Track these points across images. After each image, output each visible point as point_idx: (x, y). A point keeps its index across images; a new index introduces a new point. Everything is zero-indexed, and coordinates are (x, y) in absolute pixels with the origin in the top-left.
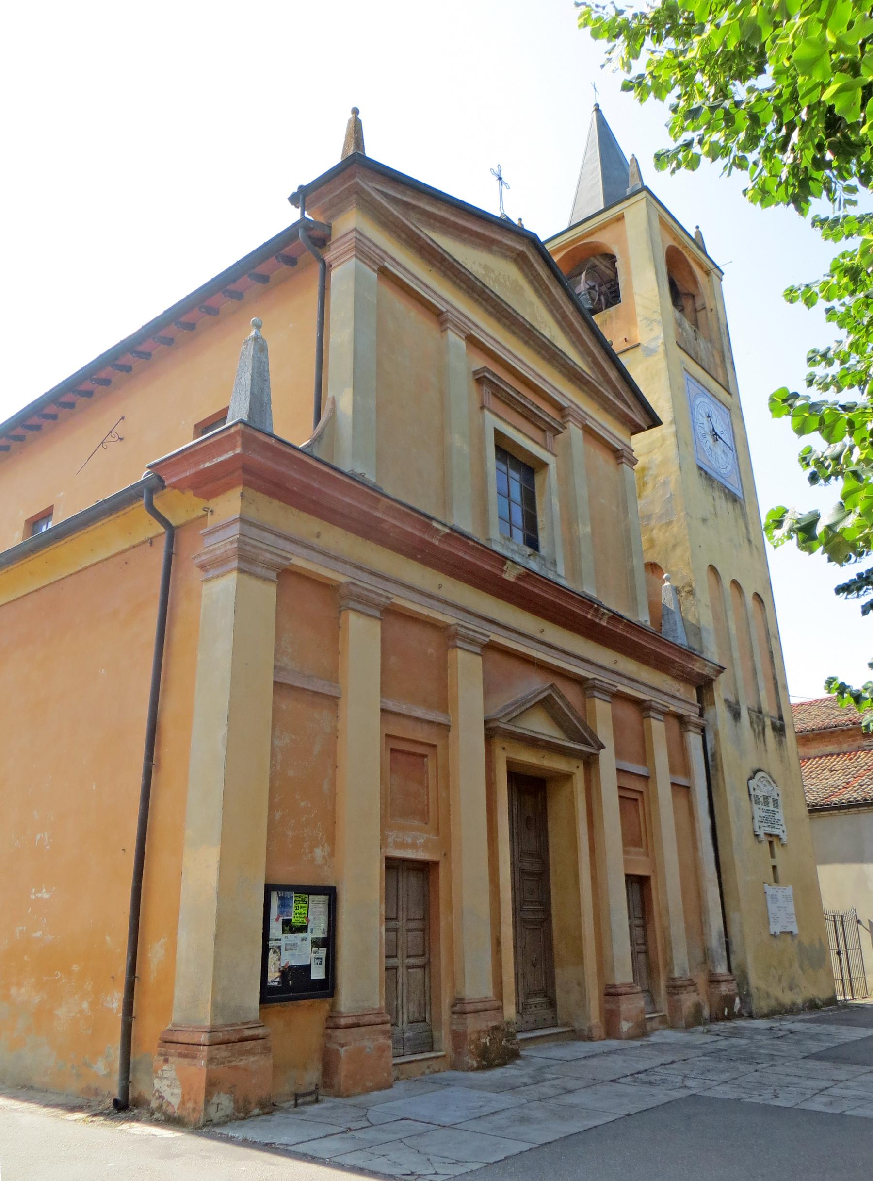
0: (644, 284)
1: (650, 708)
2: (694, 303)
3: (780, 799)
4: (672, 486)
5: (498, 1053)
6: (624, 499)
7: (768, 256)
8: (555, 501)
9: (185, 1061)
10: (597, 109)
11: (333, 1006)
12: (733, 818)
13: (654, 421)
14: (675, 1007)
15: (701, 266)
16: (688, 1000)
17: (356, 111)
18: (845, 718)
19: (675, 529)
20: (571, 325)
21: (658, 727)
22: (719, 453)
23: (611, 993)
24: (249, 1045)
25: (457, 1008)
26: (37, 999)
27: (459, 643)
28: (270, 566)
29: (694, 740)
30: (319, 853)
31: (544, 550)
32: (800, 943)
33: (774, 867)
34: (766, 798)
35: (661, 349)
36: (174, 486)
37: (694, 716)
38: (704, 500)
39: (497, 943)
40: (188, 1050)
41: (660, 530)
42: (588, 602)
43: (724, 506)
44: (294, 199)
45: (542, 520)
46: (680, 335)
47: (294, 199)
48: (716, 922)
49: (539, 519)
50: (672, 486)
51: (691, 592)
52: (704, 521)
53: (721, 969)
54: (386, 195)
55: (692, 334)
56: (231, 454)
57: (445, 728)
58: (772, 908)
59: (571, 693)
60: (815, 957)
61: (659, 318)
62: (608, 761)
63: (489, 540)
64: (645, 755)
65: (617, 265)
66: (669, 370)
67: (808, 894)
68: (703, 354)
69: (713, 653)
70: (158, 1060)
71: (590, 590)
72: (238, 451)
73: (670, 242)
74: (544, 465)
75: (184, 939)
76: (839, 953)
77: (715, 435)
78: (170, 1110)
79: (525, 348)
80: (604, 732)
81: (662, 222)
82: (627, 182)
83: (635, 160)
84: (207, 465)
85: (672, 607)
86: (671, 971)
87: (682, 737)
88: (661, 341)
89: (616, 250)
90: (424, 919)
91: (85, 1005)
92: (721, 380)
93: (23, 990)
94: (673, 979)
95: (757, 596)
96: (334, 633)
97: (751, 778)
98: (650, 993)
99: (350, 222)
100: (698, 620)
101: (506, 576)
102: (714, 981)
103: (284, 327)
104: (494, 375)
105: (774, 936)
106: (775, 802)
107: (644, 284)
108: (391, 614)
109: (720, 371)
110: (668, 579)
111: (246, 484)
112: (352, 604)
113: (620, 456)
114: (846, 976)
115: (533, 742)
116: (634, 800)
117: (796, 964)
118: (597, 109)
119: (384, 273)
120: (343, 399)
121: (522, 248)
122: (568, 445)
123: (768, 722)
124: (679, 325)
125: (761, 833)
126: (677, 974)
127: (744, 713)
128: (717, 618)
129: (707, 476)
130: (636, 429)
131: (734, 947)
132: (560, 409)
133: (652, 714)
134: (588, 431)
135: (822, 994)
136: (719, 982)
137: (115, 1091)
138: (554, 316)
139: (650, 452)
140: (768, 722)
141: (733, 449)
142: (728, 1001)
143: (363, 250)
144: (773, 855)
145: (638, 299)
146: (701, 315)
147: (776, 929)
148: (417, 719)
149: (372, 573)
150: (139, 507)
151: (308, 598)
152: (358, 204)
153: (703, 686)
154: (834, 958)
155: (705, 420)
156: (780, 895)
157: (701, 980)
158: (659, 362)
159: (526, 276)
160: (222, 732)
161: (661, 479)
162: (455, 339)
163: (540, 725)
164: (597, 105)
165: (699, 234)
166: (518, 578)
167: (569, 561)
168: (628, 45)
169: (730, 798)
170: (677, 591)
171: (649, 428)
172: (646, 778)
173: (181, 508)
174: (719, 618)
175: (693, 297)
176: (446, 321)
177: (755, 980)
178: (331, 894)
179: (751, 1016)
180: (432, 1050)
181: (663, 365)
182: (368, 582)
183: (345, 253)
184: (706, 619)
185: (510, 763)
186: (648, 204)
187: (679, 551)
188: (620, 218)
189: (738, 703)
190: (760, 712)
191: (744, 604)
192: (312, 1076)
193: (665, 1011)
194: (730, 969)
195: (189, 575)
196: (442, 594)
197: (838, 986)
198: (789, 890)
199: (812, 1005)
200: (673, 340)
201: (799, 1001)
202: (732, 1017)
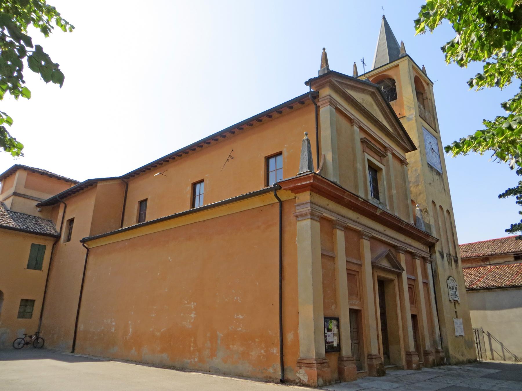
0: (406, 92)
1: (363, 234)
2: (423, 96)
3: (457, 287)
4: (419, 171)
5: (381, 373)
6: (404, 177)
7: (463, 100)
8: (385, 183)
9: (308, 369)
10: (384, 18)
11: (340, 354)
12: (442, 294)
13: (414, 148)
14: (427, 361)
15: (425, 82)
16: (431, 358)
17: (324, 49)
18: (475, 254)
19: (420, 188)
20: (388, 116)
21: (418, 262)
22: (434, 156)
23: (408, 354)
24: (325, 365)
25: (370, 357)
26: (241, 349)
27: (364, 237)
28: (318, 217)
29: (429, 266)
30: (333, 307)
31: (381, 200)
32: (465, 339)
33: (456, 312)
34: (453, 287)
35: (414, 118)
36: (284, 189)
37: (429, 258)
38: (430, 176)
39: (378, 336)
40: (309, 365)
41: (414, 187)
42: (400, 220)
43: (436, 177)
44: (307, 83)
45: (380, 189)
46: (420, 112)
47: (307, 83)
48: (437, 331)
49: (379, 189)
50: (419, 171)
51: (427, 211)
52: (430, 184)
53: (440, 348)
54: (337, 81)
55: (423, 110)
56: (308, 182)
57: (360, 265)
58: (456, 326)
59: (393, 251)
60: (470, 345)
61: (413, 107)
62: (405, 275)
63: (368, 199)
64: (360, 256)
65: (396, 84)
66: (417, 127)
67: (467, 321)
68: (427, 118)
69: (435, 234)
70: (297, 368)
71: (396, 214)
72: (312, 181)
73: (416, 75)
74: (381, 169)
75: (302, 333)
76: (477, 343)
77: (433, 150)
78: (304, 382)
79: (380, 132)
80: (403, 265)
81: (413, 68)
82: (399, 52)
83: (402, 43)
84: (299, 184)
85: (420, 217)
86: (425, 348)
87: (424, 265)
88: (414, 116)
89: (395, 79)
90: (357, 328)
91: (262, 351)
92: (433, 127)
93: (235, 346)
94: (426, 351)
95: (448, 211)
96: (332, 236)
97: (448, 279)
98: (419, 355)
99: (326, 92)
100: (429, 222)
101: (377, 213)
102: (438, 352)
103: (301, 126)
104: (368, 140)
105: (457, 337)
106: (456, 288)
107: (406, 92)
108: (347, 229)
109: (433, 123)
110: (418, 206)
111: (311, 190)
112: (337, 227)
113: (403, 162)
114: (480, 352)
115: (384, 269)
116: (412, 288)
117: (464, 348)
118: (384, 18)
119: (337, 109)
120: (328, 156)
121: (373, 90)
122: (388, 161)
123: (453, 259)
124: (419, 107)
125: (451, 299)
126: (427, 349)
127: (445, 256)
128: (435, 221)
129: (430, 167)
130: (408, 151)
131: (444, 340)
132: (385, 147)
133: (364, 237)
134: (394, 155)
135: (473, 358)
136: (411, 355)
137: (280, 377)
138: (382, 113)
139: (410, 158)
140: (453, 259)
141: (439, 155)
142: (442, 359)
143: (332, 103)
144: (455, 308)
145: (404, 98)
146: (425, 101)
147: (457, 334)
148: (354, 263)
149: (341, 216)
150: (272, 194)
151: (328, 225)
152: (329, 86)
153: (431, 246)
154: (476, 345)
155: (428, 144)
156: (458, 322)
157: (434, 351)
158: (413, 123)
159: (374, 100)
160: (310, 270)
161: (414, 168)
162: (356, 128)
163: (385, 264)
164: (384, 16)
165: (424, 68)
166: (381, 214)
167: (390, 204)
168: (483, 132)
169: (442, 287)
170: (421, 211)
171: (412, 151)
172: (414, 280)
173: (285, 195)
174: (436, 221)
175: (422, 94)
176: (353, 122)
177: (451, 352)
178: (338, 320)
179: (450, 364)
180: (362, 370)
181: (415, 125)
182: (341, 219)
183: (325, 103)
184: (432, 222)
185: (378, 277)
186: (408, 61)
187: (421, 196)
188: (397, 66)
189: (443, 252)
190: (450, 255)
191: (443, 214)
192: (336, 376)
193: (423, 362)
194: (442, 348)
195: (289, 218)
196: (358, 220)
197: (478, 356)
198: (461, 320)
199: (470, 362)
200: (418, 115)
201: (465, 360)
202: (444, 364)
